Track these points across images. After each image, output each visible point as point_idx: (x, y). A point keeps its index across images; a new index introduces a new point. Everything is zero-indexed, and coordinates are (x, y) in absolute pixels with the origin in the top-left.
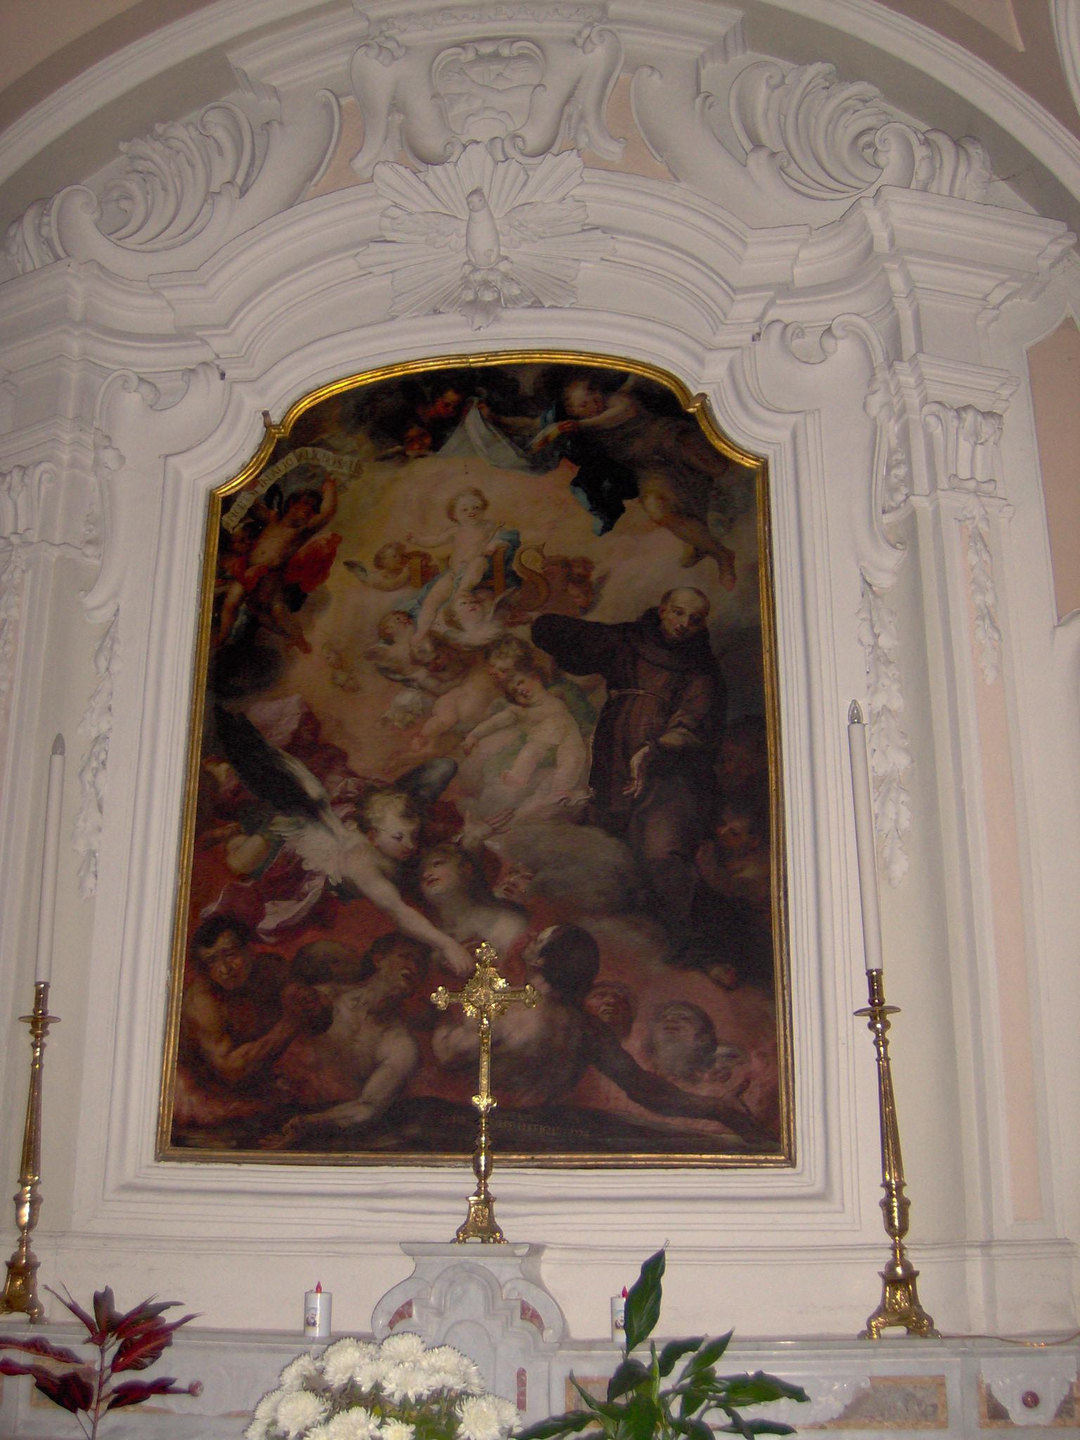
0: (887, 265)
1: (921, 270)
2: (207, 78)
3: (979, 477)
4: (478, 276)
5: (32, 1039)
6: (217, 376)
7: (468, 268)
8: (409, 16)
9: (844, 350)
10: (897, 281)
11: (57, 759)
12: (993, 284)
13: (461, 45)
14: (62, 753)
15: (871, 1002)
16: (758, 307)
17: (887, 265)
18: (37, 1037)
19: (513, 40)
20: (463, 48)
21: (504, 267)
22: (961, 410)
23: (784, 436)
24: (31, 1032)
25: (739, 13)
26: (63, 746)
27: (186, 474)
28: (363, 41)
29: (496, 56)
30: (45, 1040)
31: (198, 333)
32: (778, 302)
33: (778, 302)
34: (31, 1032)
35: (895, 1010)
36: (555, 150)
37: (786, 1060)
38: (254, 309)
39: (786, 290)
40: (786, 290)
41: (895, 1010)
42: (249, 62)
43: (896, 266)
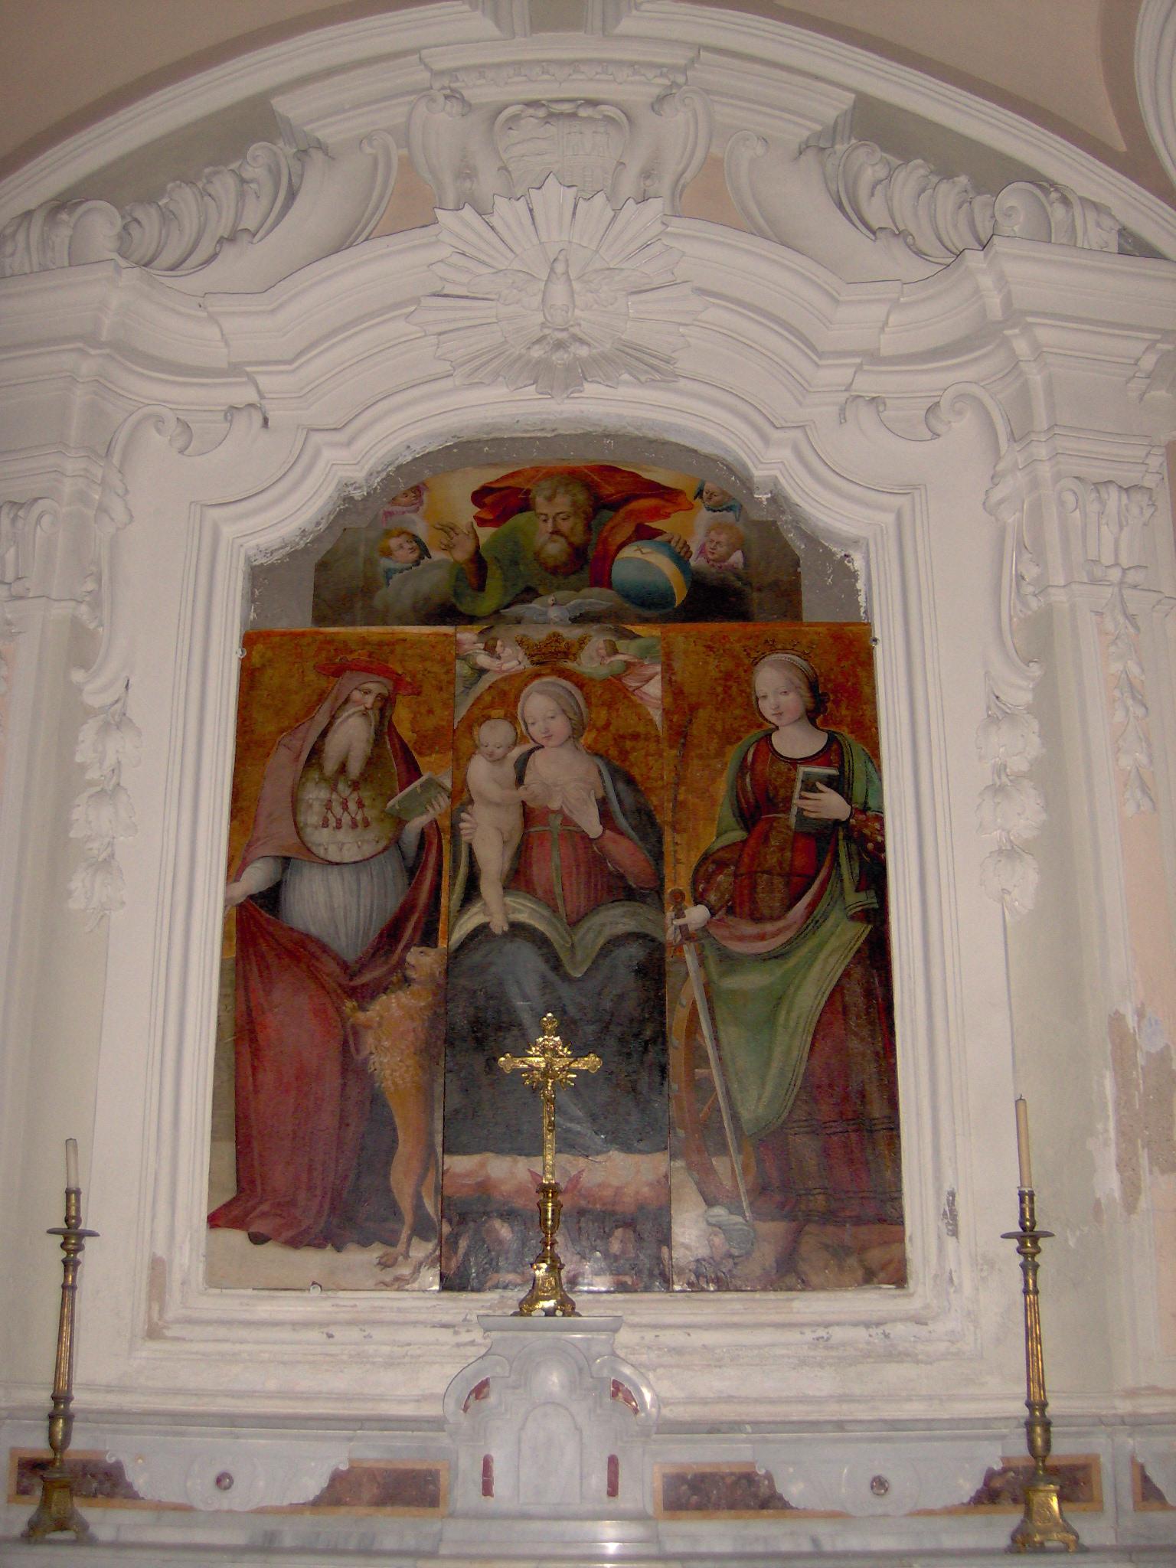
0: (1008, 332)
1: (1043, 335)
2: (253, 123)
3: (1125, 562)
5: (1020, 1259)
6: (260, 421)
9: (963, 428)
10: (1021, 346)
17: (1008, 332)
18: (69, 1252)
22: (1100, 485)
23: (890, 518)
24: (63, 1245)
27: (228, 531)
28: (424, 92)
29: (573, 115)
30: (1037, 1258)
31: (248, 369)
32: (866, 367)
33: (866, 367)
36: (552, 976)
38: (316, 374)
40: (874, 357)
42: (282, 105)
43: (1017, 331)
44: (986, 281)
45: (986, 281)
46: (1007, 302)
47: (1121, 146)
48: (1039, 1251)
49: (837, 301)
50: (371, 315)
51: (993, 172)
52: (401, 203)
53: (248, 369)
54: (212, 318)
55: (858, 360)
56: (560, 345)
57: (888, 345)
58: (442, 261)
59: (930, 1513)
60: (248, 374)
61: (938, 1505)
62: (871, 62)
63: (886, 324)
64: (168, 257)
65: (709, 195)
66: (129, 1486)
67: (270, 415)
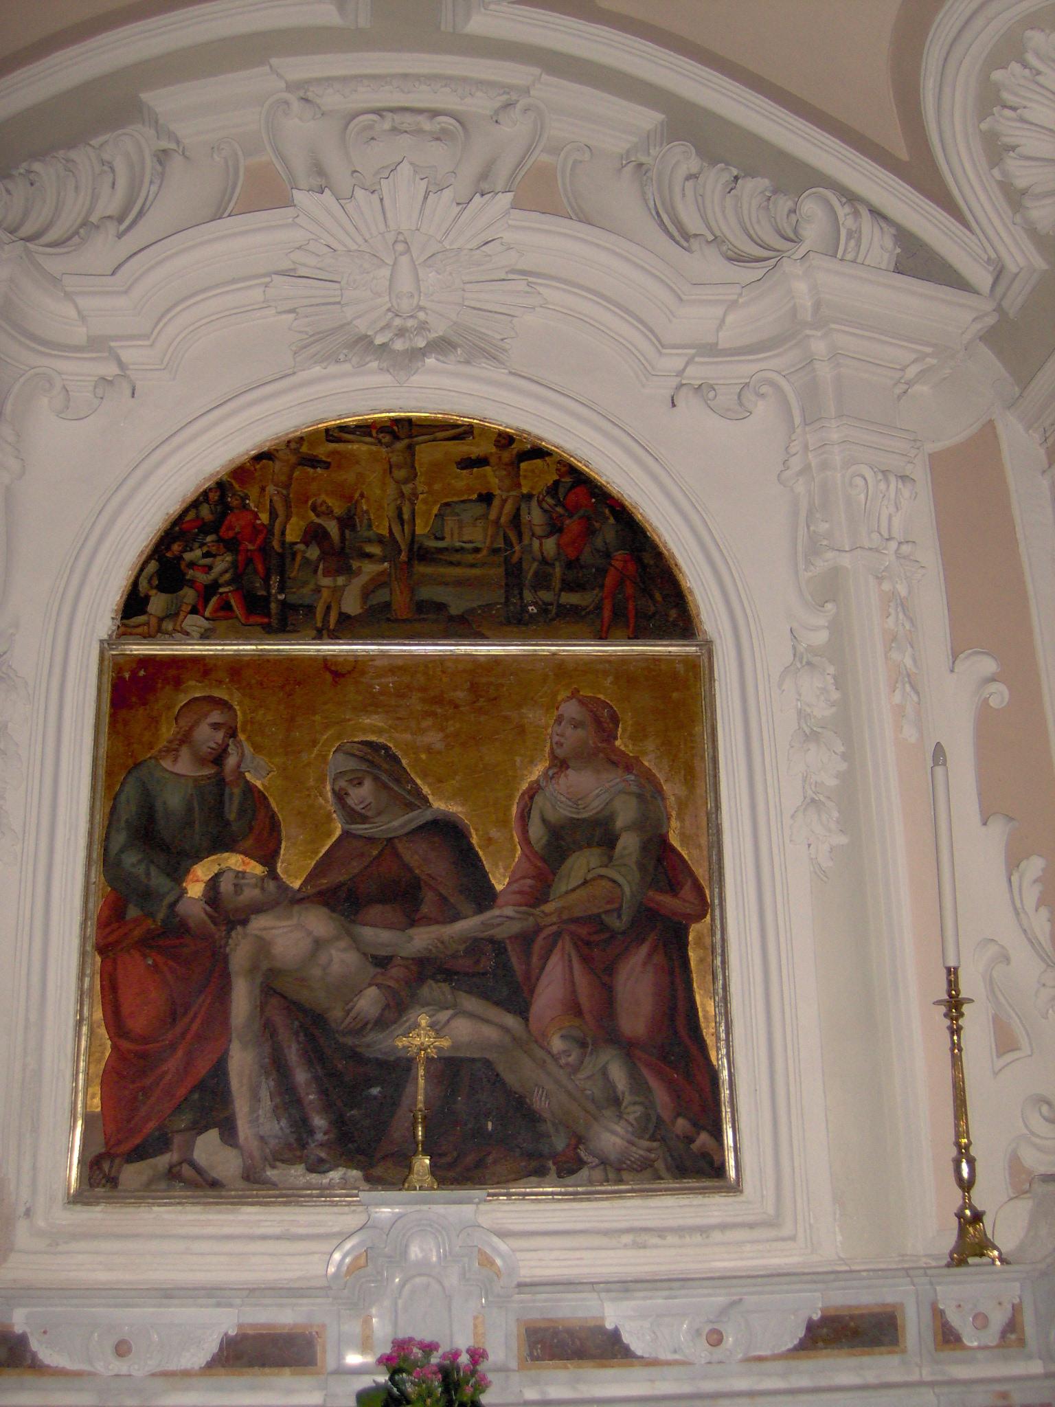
4: (398, 322)
5: (947, 1022)
6: (128, 392)
7: (390, 315)
8: (329, 80)
11: (939, 770)
12: (914, 356)
13: (378, 112)
14: (945, 764)
15: (950, 996)
16: (678, 363)
18: (952, 1019)
19: (434, 113)
20: (381, 116)
21: (421, 315)
24: (946, 1015)
25: (660, 117)
26: (944, 755)
30: (961, 1022)
31: (112, 344)
34: (946, 1015)
35: (970, 1001)
37: (248, 1197)
38: (209, 350)
39: (711, 350)
40: (711, 350)
41: (970, 1001)
43: (819, 334)
44: (801, 287)
45: (801, 287)
46: (817, 305)
47: (903, 154)
48: (962, 1015)
49: (681, 299)
50: (603, 296)
51: (793, 177)
52: (259, 190)
53: (112, 344)
54: (68, 296)
55: (692, 351)
56: (401, 332)
57: (726, 339)
58: (299, 248)
59: (760, 1359)
60: (111, 348)
61: (767, 1353)
62: (689, 68)
63: (723, 321)
64: (24, 232)
65: (543, 190)
66: (34, 1356)
67: (138, 385)
